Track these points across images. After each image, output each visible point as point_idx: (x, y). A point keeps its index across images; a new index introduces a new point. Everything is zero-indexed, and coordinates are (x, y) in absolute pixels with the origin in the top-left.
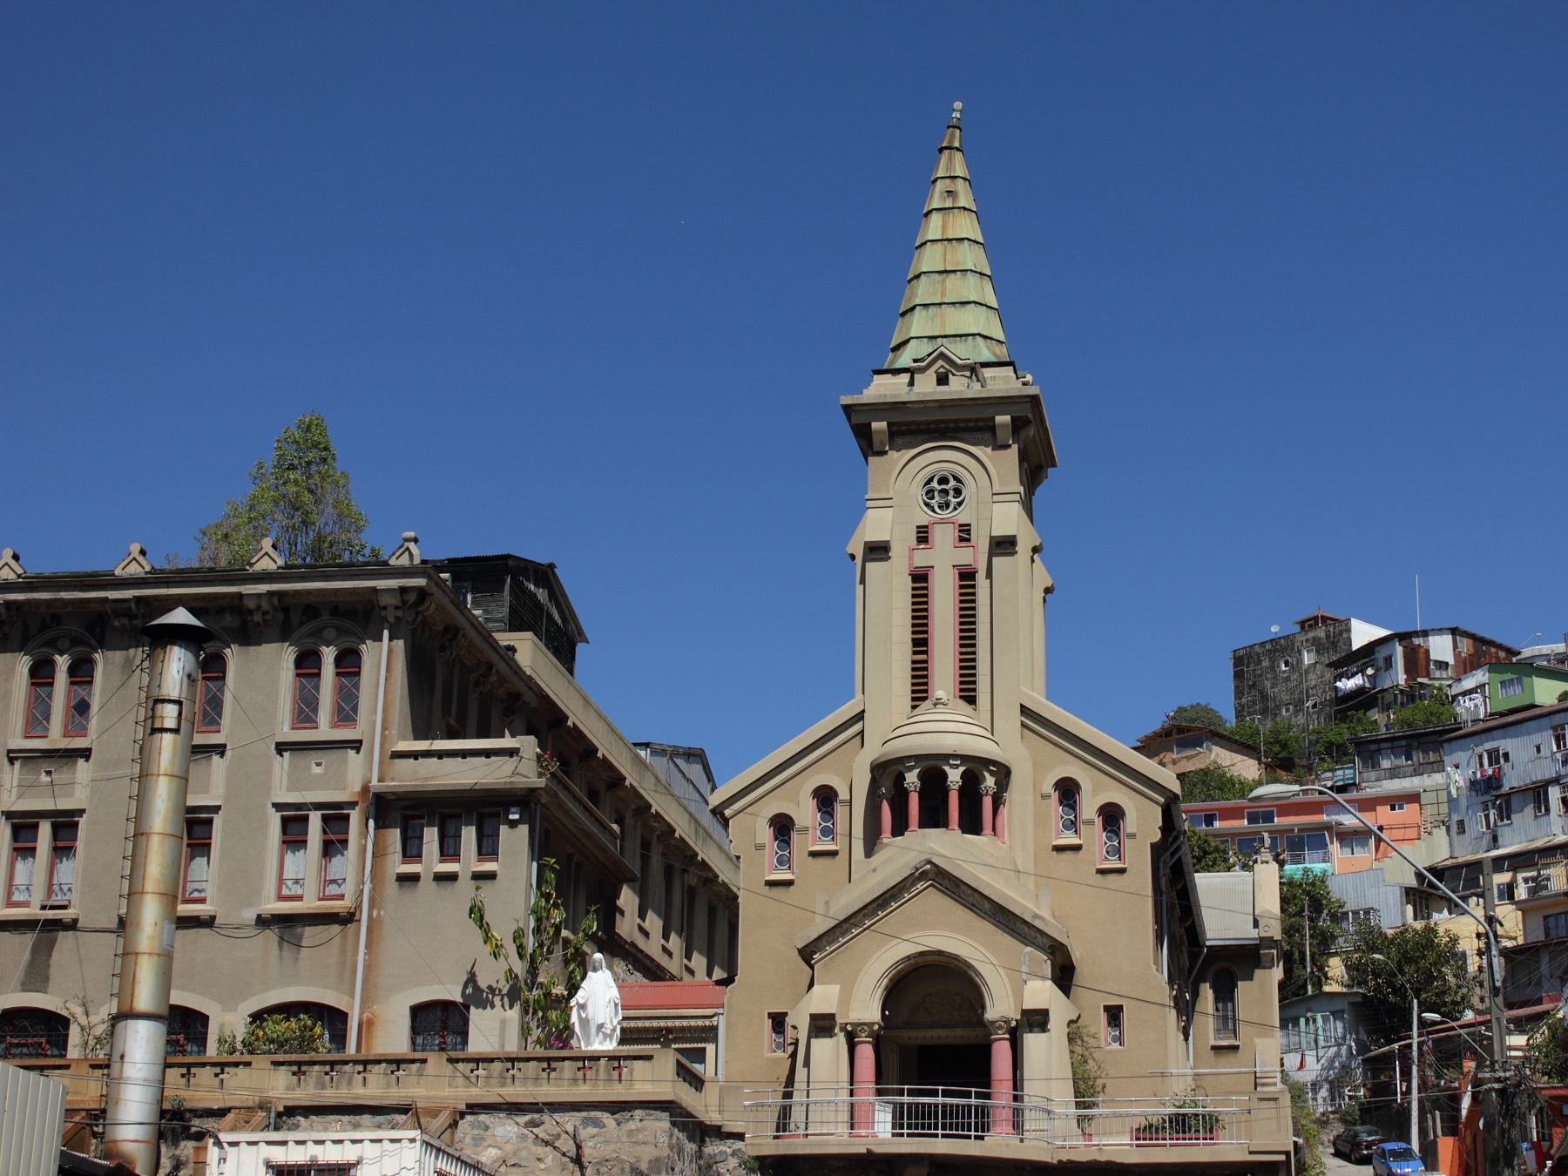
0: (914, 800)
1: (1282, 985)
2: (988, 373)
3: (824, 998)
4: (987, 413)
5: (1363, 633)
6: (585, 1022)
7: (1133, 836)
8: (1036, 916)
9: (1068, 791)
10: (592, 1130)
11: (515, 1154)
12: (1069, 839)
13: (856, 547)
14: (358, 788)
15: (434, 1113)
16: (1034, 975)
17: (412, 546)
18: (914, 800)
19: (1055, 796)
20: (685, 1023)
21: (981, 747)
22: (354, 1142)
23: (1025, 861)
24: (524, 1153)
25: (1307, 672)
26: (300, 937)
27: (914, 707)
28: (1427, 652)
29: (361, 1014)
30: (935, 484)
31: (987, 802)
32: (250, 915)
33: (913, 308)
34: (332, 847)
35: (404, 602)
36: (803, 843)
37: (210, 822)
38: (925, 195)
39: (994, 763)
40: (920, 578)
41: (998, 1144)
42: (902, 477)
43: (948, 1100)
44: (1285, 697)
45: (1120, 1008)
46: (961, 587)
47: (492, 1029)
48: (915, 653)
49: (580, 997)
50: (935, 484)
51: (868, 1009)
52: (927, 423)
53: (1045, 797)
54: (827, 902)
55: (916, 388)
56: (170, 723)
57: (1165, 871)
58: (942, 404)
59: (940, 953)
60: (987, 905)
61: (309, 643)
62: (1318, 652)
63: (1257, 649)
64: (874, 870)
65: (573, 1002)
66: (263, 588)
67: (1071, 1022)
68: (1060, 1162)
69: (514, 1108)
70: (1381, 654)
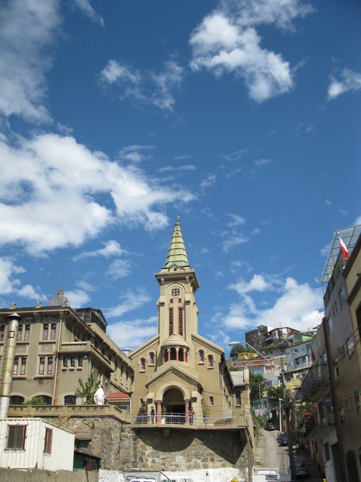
0: (169, 354)
1: (251, 394)
2: (185, 268)
3: (150, 395)
4: (184, 276)
5: (269, 329)
6: (97, 399)
7: (215, 361)
8: (194, 378)
9: (201, 352)
10: (96, 422)
11: (81, 426)
12: (202, 362)
13: (157, 304)
14: (54, 352)
15: (63, 417)
16: (194, 390)
17: (66, 303)
18: (169, 354)
19: (199, 354)
20: (123, 401)
22: (27, 420)
23: (193, 366)
24: (82, 426)
26: (43, 382)
27: (170, 336)
28: (282, 332)
29: (54, 398)
30: (174, 291)
31: (185, 355)
32: (33, 377)
33: (170, 256)
34: (50, 363)
35: (65, 314)
37: (26, 359)
38: (173, 234)
39: (186, 347)
40: (171, 310)
41: (187, 425)
42: (167, 290)
44: (255, 342)
45: (213, 397)
46: (179, 311)
47: (79, 401)
48: (170, 325)
49: (96, 394)
50: (174, 291)
51: (160, 398)
52: (172, 278)
53: (197, 354)
54: (151, 376)
55: (170, 271)
56: (12, 336)
57: (223, 368)
58: (175, 274)
59: (174, 386)
60: (184, 376)
61: (46, 322)
62: (261, 333)
65: (94, 395)
66: (37, 311)
67: (202, 400)
68: (198, 429)
69: (81, 417)
70: (273, 333)
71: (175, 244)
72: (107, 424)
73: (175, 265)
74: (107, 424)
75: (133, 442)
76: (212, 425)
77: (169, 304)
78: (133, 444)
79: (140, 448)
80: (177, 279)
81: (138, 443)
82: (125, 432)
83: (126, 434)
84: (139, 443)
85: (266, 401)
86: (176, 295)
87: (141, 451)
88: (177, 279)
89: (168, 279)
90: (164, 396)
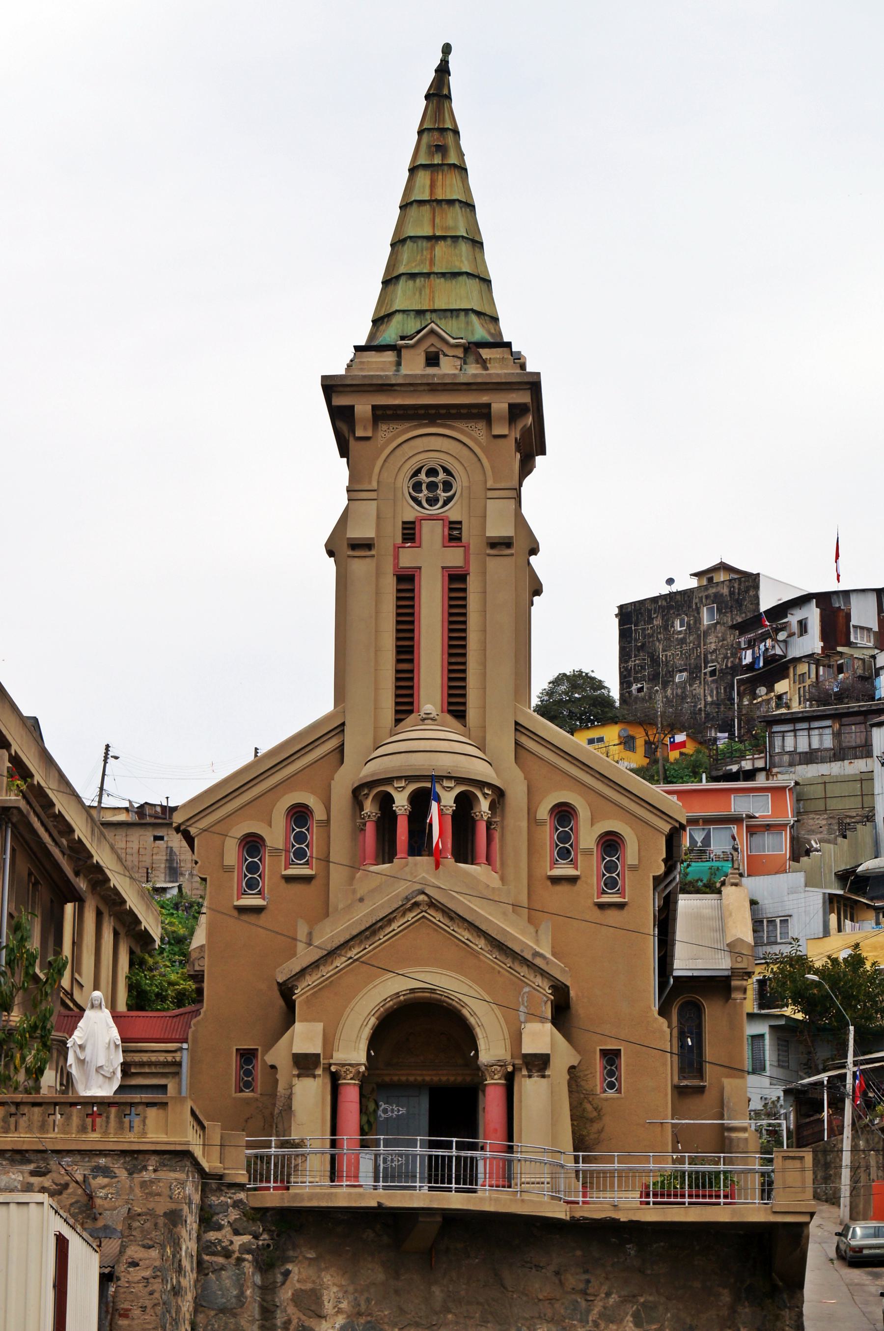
4: (484, 399)
8: (537, 954)
10: (101, 1180)
12: (564, 870)
21: (481, 770)
25: (706, 634)
28: (848, 617)
30: (422, 476)
31: (482, 828)
36: (272, 868)
40: (407, 582)
41: (486, 1198)
43: (463, 1153)
44: (679, 662)
45: (617, 1053)
49: (77, 1037)
50: (422, 476)
51: (354, 1052)
55: (404, 370)
59: (432, 991)
62: (719, 610)
63: (648, 605)
64: (361, 900)
71: (426, 209)
72: (159, 1194)
73: (432, 332)
74: (159, 1194)
75: (258, 1279)
76: (632, 1198)
77: (397, 548)
78: (260, 1288)
79: (291, 1309)
80: (443, 411)
81: (283, 1283)
82: (219, 1228)
83: (224, 1235)
84: (288, 1283)
85: (762, 1036)
86: (432, 501)
87: (295, 1321)
88: (443, 411)
89: (389, 412)
90: (374, 1041)
